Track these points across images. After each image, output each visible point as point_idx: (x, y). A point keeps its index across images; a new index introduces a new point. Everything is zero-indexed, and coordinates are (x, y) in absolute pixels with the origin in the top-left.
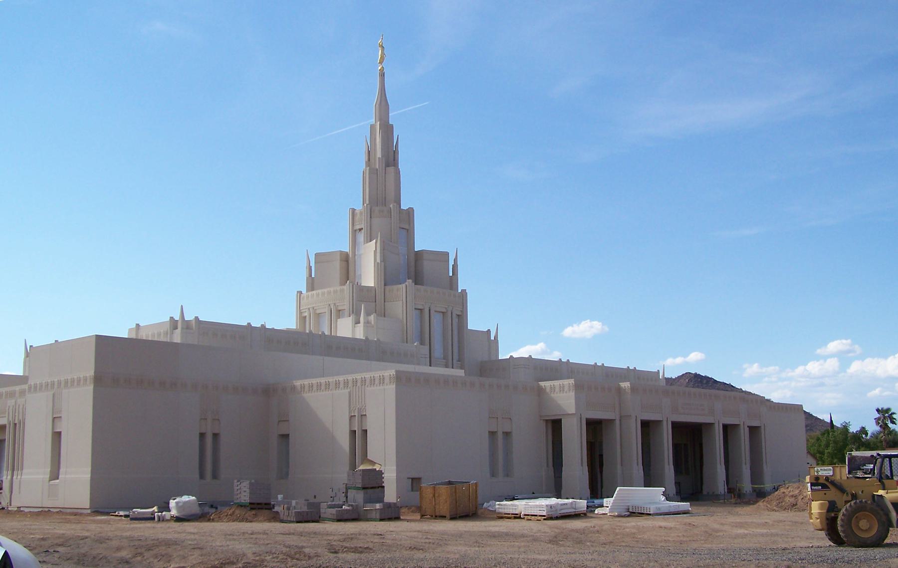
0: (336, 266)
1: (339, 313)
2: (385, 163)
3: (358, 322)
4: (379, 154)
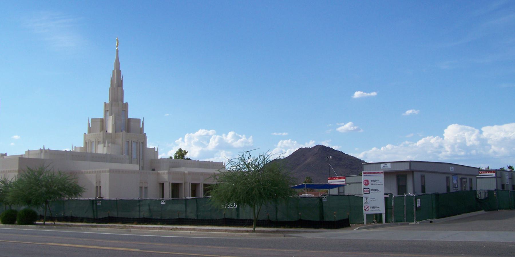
0: (99, 124)
1: (99, 142)
2: (117, 85)
3: (105, 146)
4: (115, 82)
